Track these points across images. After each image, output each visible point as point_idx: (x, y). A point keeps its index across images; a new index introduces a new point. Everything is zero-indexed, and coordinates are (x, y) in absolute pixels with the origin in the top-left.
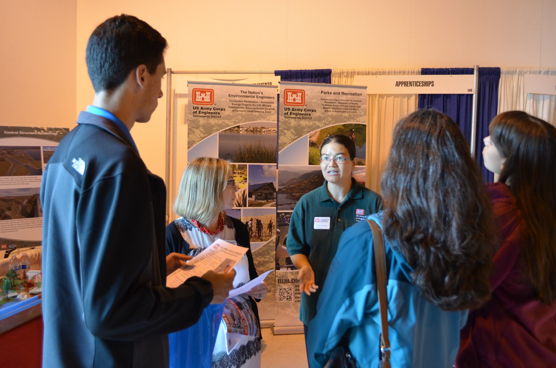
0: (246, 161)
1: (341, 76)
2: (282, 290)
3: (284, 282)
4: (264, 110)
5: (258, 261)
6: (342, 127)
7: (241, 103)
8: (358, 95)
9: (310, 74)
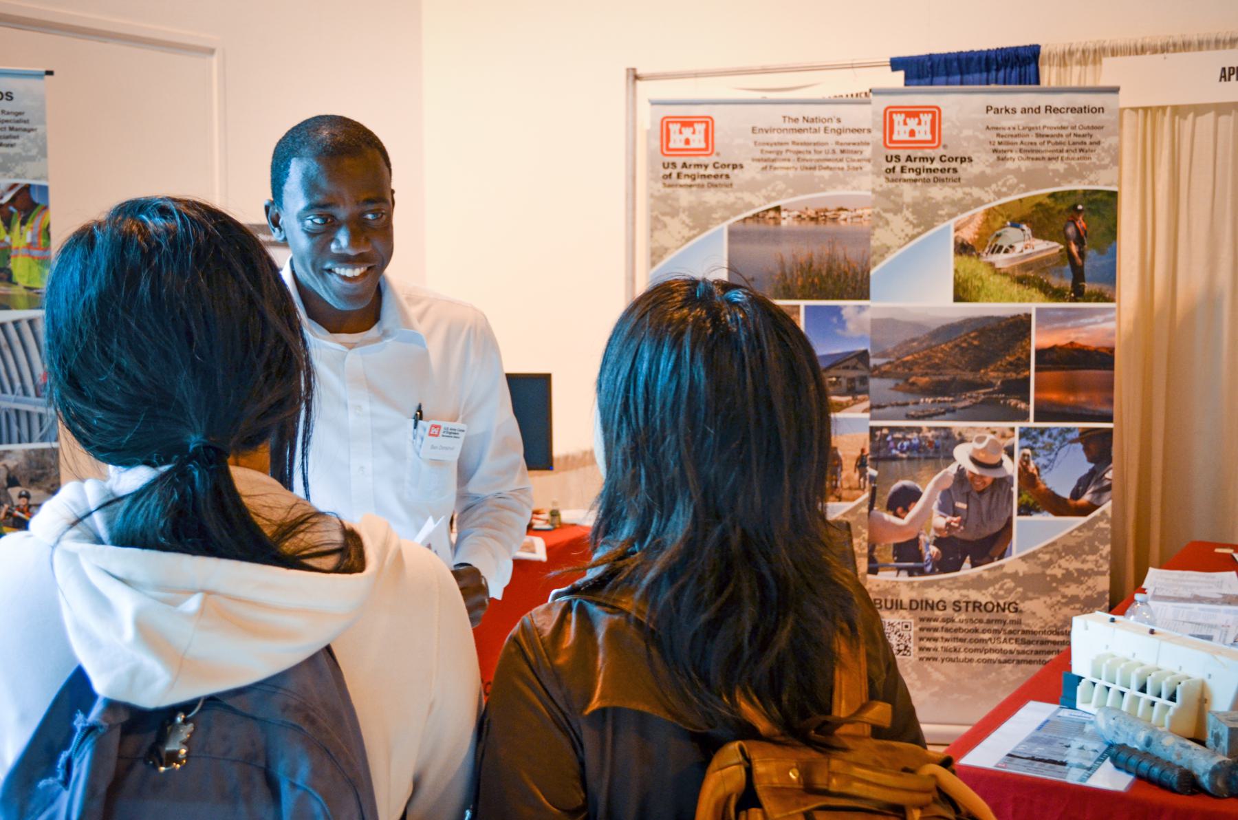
0: (799, 296)
1: (1068, 62)
2: (909, 629)
3: (889, 605)
4: (844, 165)
5: (1064, 569)
6: (1048, 201)
7: (783, 148)
8: (1094, 110)
9: (983, 62)
